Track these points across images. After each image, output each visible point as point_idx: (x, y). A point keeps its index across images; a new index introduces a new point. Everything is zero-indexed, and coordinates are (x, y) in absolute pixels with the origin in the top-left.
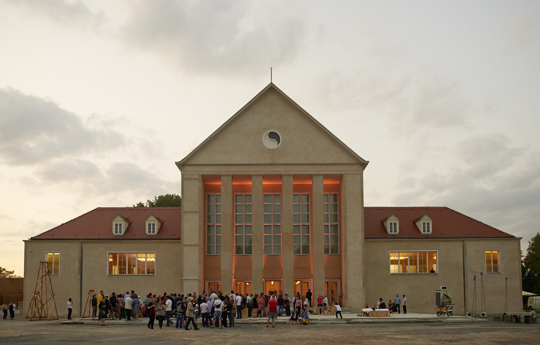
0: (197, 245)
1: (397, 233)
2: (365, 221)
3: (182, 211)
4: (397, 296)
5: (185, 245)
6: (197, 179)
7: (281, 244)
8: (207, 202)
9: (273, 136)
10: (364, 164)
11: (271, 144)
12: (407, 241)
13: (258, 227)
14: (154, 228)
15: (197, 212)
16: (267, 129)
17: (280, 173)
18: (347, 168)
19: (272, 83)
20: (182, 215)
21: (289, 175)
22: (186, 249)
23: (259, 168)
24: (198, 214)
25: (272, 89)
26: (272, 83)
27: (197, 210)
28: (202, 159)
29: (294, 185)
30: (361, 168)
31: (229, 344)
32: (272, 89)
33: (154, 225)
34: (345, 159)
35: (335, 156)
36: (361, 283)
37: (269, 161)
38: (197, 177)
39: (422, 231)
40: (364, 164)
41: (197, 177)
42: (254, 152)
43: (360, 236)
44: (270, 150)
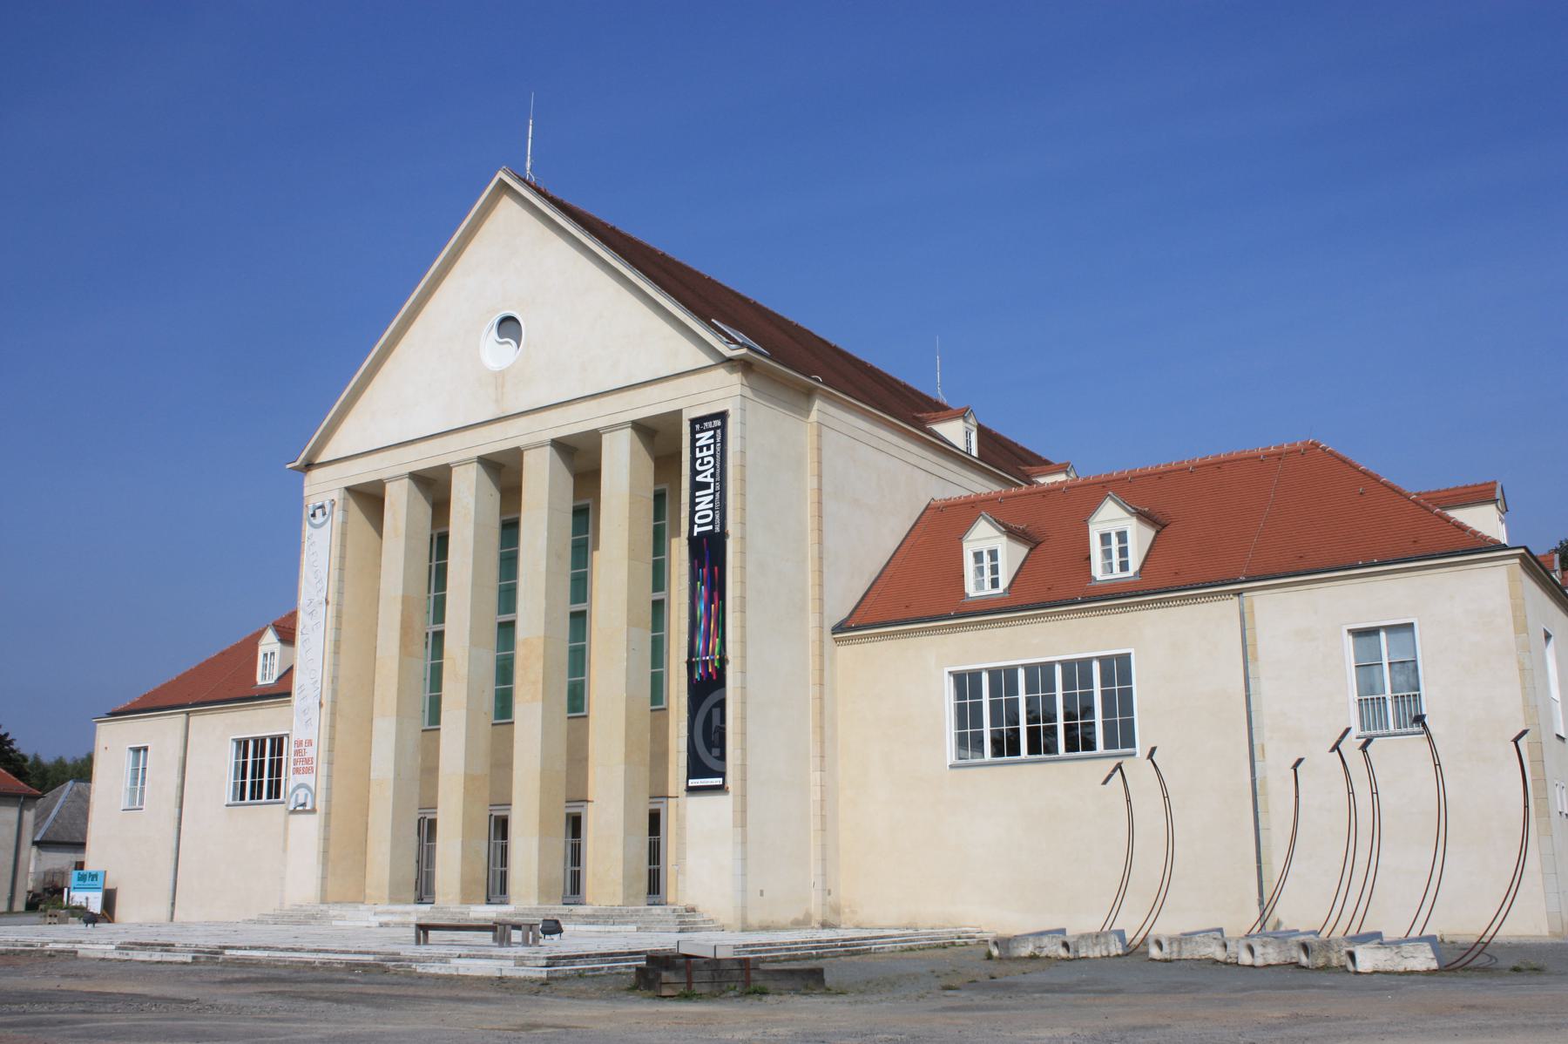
9: (509, 326)
11: (496, 354)
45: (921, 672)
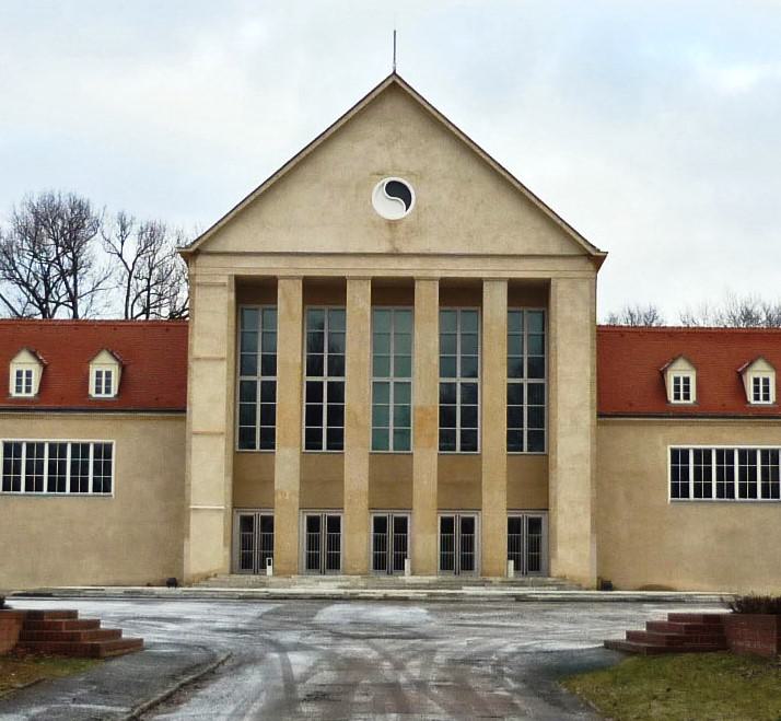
0: (222, 433)
1: (771, 402)
2: (599, 382)
3: (189, 357)
5: (196, 434)
6: (224, 285)
7: (670, 498)
8: (239, 327)
9: (397, 190)
10: (596, 259)
11: (392, 209)
12: (709, 424)
13: (426, 458)
14: (29, 382)
15: (222, 359)
16: (381, 174)
17: (411, 274)
18: (560, 265)
19: (394, 73)
20: (190, 363)
21: (432, 279)
23: (364, 263)
24: (225, 363)
25: (394, 88)
26: (394, 73)
27: (224, 354)
28: (235, 241)
30: (591, 267)
32: (394, 88)
33: (29, 374)
34: (554, 246)
37: (384, 248)
38: (225, 280)
39: (751, 398)
40: (596, 259)
41: (225, 280)
43: (587, 416)
44: (392, 224)
45: (657, 445)
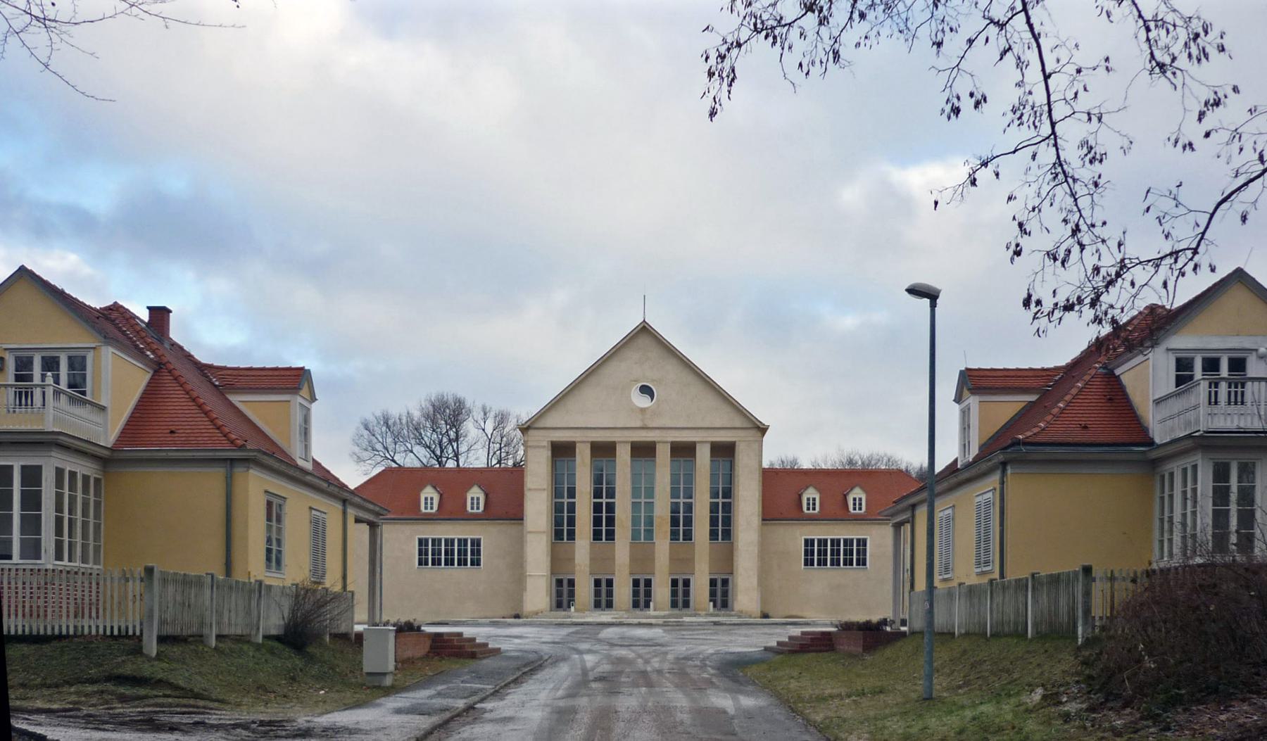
4: (949, 118)
9: (646, 390)
10: (763, 430)
11: (643, 402)
16: (637, 381)
18: (742, 433)
22: (529, 538)
23: (626, 433)
25: (644, 330)
28: (550, 421)
29: (39, 558)
30: (759, 434)
31: (531, 703)
32: (644, 330)
34: (738, 422)
35: (722, 417)
36: (755, 581)
37: (639, 424)
40: (763, 430)
41: (545, 444)
42: (616, 414)
43: (756, 520)
44: (643, 410)
